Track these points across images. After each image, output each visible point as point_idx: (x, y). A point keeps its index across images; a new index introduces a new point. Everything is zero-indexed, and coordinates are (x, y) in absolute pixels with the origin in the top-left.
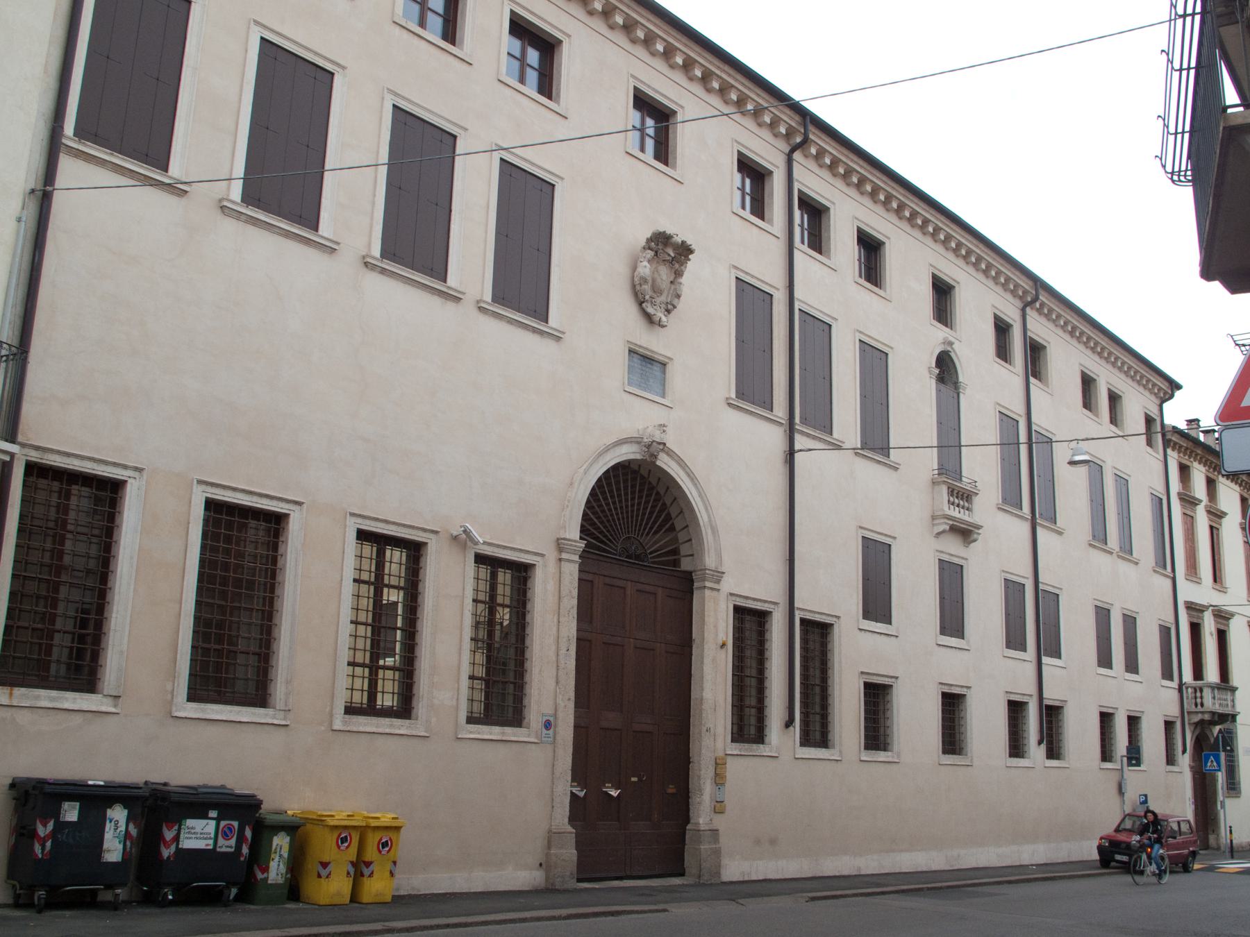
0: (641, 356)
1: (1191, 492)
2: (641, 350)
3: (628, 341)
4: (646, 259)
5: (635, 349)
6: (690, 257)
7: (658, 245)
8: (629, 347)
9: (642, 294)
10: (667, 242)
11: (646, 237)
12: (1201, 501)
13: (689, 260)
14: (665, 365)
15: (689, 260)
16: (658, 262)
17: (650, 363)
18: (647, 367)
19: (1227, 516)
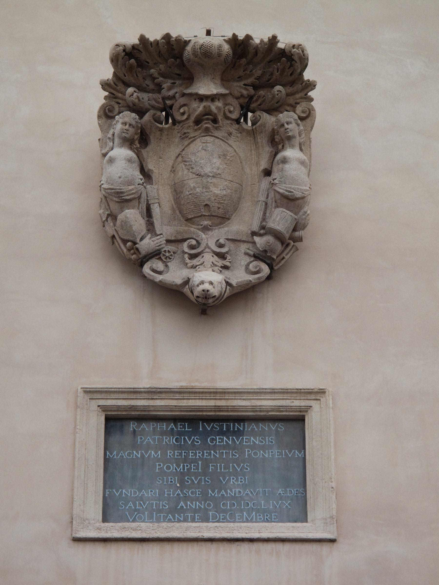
0: (175, 420)
1: (229, 289)
2: (159, 403)
3: (87, 391)
4: (116, 140)
5: (132, 408)
6: (308, 75)
7: (159, 88)
8: (103, 408)
9: (125, 242)
10: (182, 65)
11: (309, 78)
12: (109, 113)
13: (311, 85)
14: (301, 420)
15: (311, 85)
16: (184, 136)
17: (222, 433)
18: (214, 448)
19: (237, 34)
